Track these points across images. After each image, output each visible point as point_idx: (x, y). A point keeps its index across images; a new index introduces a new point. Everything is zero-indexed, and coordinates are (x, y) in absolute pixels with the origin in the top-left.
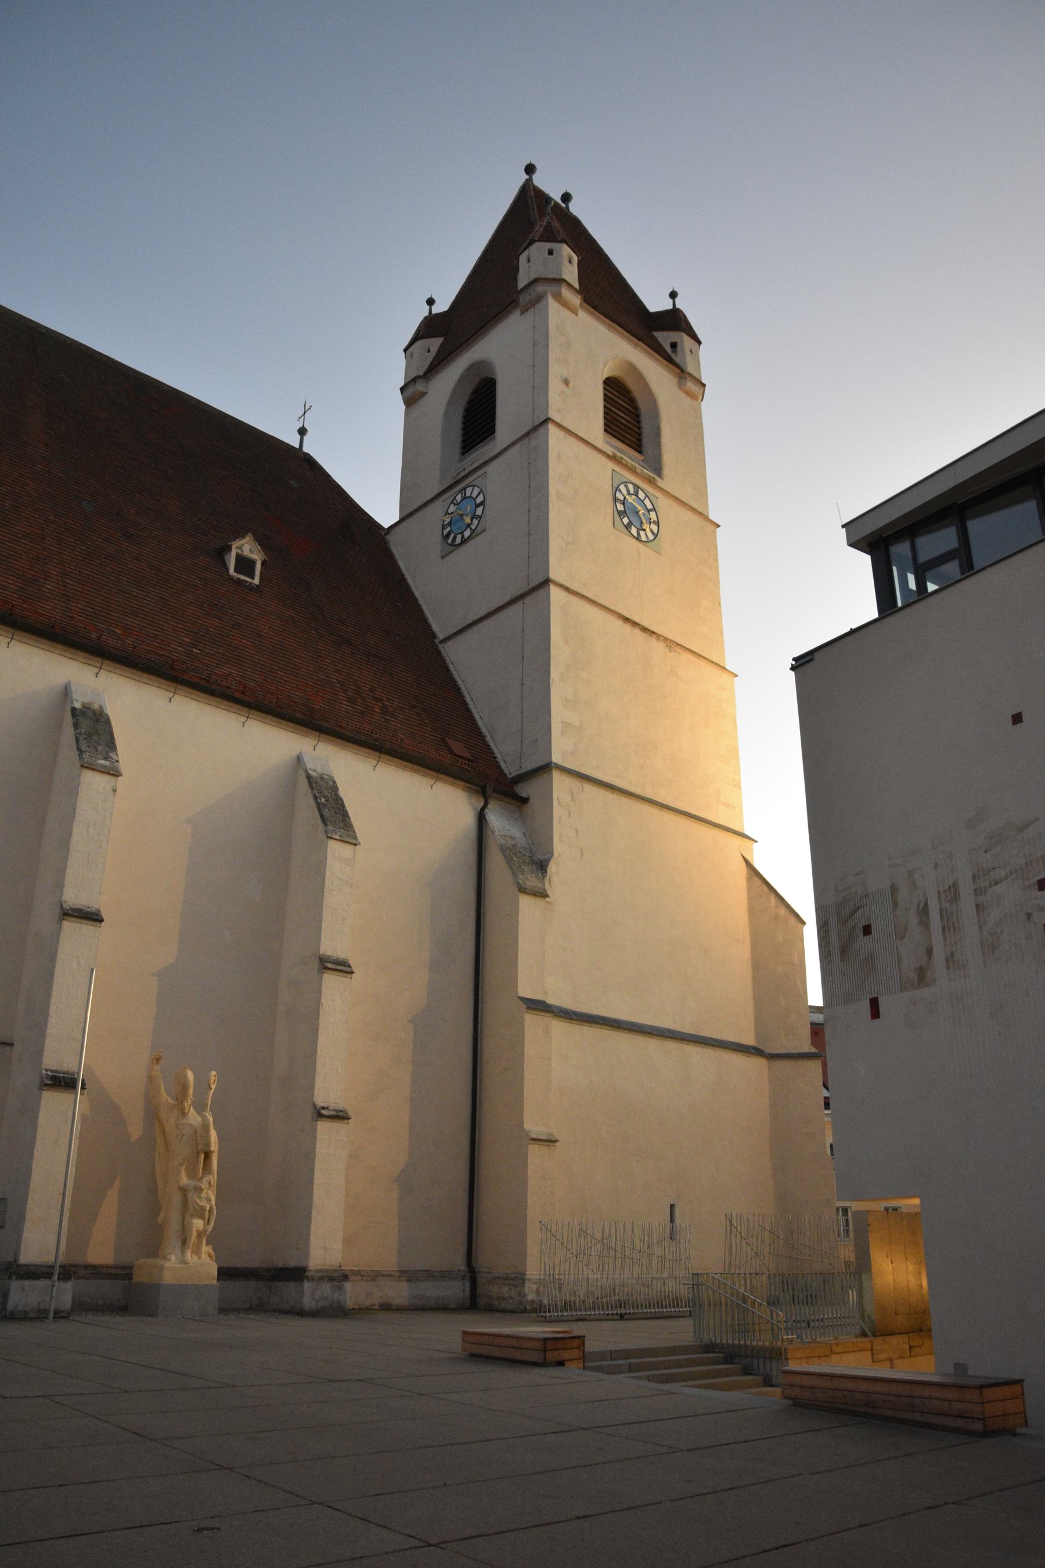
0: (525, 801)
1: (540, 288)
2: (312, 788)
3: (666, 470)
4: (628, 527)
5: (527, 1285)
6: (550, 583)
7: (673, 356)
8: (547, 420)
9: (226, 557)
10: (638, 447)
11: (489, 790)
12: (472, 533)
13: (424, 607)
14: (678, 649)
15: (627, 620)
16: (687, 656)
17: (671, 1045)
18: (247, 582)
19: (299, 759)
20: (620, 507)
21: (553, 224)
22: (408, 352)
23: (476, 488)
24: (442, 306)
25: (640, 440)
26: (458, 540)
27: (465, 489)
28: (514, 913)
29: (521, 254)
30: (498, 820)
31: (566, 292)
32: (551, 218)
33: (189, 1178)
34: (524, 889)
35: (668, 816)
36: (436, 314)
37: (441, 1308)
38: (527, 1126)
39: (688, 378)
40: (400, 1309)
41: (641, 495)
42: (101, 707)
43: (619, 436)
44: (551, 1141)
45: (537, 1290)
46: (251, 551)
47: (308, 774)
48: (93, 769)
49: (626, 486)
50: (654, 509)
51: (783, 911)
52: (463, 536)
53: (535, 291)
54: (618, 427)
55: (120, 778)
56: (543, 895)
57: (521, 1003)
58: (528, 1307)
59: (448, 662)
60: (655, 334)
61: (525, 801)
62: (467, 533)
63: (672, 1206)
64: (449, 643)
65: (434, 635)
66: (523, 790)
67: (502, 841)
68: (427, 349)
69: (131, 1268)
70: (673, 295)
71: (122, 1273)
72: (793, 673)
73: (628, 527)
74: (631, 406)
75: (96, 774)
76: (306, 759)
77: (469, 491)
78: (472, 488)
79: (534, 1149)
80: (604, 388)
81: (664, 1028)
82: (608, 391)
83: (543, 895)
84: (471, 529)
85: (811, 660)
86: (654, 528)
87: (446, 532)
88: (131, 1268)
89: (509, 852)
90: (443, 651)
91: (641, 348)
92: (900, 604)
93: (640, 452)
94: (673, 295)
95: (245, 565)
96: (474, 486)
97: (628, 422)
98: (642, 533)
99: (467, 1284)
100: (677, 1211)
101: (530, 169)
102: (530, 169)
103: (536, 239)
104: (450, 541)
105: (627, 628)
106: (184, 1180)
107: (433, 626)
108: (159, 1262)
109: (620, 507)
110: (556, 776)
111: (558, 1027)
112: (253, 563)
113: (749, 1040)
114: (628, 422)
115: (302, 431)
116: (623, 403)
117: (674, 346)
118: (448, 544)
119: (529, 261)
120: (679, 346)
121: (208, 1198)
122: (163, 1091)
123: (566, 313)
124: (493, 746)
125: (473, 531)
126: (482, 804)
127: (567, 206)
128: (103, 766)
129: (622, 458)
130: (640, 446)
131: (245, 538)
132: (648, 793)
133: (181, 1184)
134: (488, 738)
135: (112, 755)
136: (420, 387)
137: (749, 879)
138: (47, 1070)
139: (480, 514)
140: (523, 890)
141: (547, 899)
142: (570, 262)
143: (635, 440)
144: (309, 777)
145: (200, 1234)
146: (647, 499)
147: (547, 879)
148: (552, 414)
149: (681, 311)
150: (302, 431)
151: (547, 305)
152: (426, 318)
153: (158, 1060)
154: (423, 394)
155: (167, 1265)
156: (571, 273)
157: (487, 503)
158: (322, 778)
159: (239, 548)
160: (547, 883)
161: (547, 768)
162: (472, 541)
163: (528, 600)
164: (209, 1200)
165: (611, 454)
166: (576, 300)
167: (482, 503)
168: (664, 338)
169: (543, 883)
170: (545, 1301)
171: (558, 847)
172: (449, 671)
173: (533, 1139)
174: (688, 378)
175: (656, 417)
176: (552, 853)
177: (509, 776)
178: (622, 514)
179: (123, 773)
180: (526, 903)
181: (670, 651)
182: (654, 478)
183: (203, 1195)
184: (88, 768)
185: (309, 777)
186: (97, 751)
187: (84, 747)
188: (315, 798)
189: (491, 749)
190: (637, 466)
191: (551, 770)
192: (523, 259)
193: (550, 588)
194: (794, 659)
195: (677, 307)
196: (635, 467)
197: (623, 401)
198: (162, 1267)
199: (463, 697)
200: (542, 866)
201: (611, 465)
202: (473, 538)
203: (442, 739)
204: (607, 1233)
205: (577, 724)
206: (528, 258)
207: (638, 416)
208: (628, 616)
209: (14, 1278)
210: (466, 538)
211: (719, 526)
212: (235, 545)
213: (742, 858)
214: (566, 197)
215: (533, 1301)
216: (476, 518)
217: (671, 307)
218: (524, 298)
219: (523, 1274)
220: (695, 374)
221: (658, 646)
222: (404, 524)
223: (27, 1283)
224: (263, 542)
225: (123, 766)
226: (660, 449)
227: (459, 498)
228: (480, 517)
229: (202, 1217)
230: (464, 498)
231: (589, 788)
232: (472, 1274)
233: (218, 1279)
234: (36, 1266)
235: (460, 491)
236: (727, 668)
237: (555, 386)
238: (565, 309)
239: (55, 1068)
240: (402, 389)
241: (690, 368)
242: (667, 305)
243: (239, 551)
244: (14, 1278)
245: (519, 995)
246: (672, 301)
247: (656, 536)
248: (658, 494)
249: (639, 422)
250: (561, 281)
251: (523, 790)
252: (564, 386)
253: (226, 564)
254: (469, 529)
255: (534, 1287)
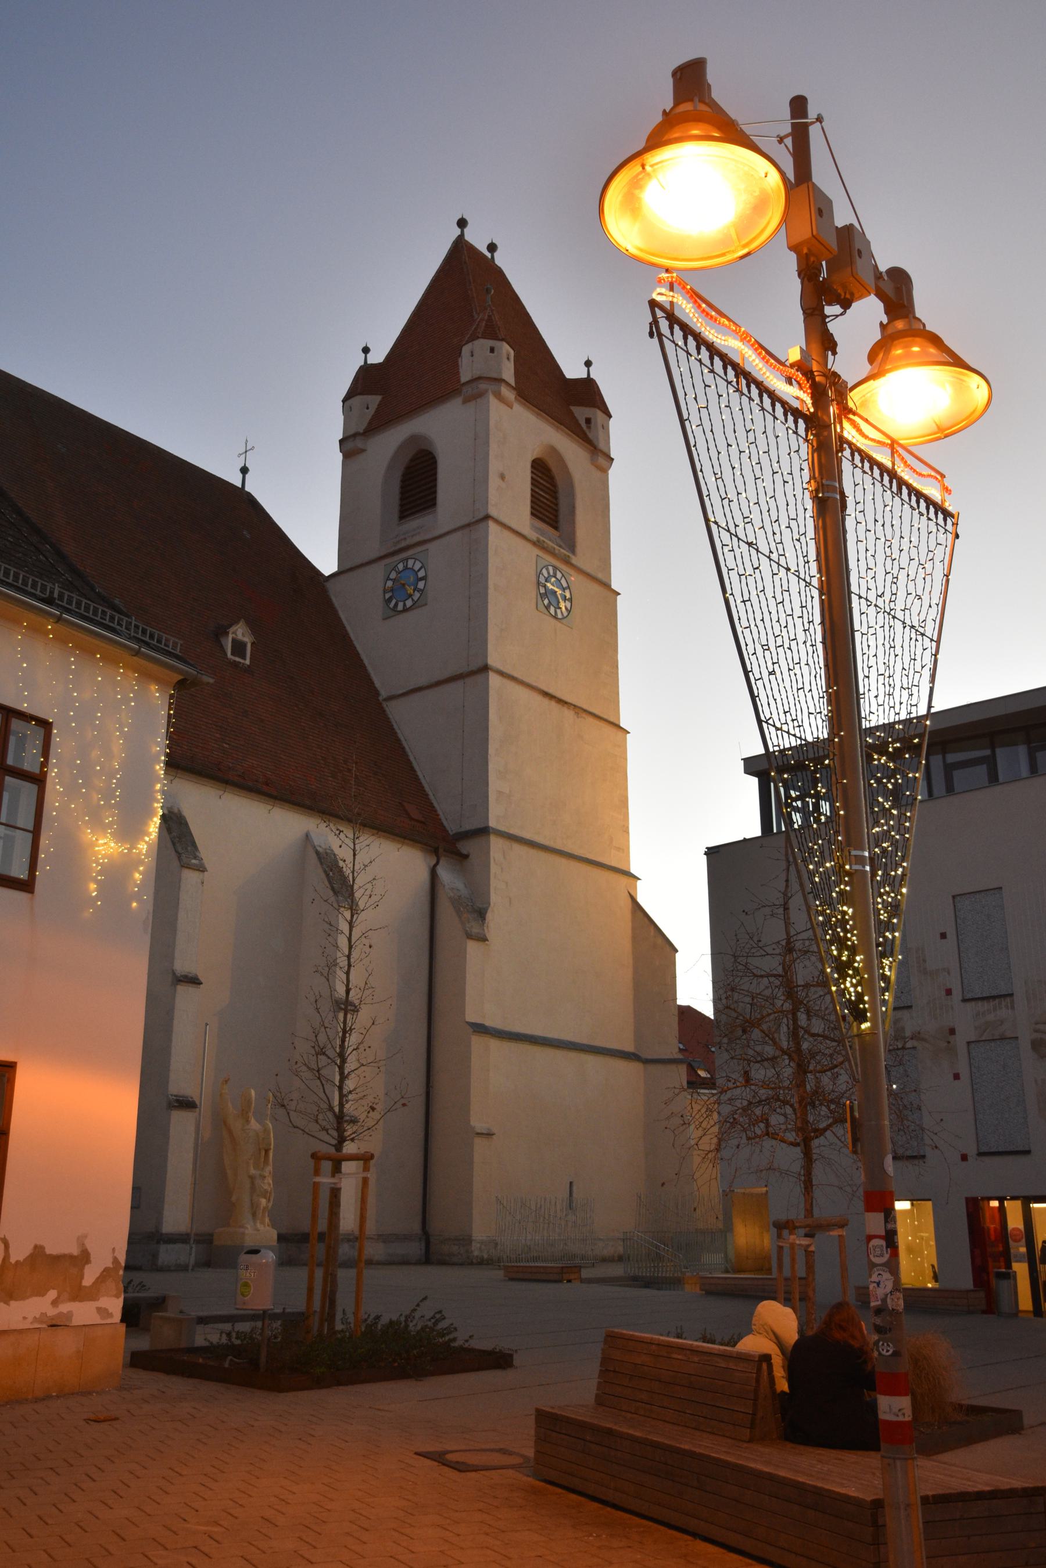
0: (466, 857)
1: (483, 386)
2: (321, 864)
3: (579, 548)
4: (547, 608)
5: (474, 1244)
6: (490, 672)
7: (588, 433)
8: (487, 517)
9: (223, 640)
10: (554, 524)
11: (441, 851)
12: (414, 604)
13: (366, 662)
14: (584, 715)
15: (546, 694)
16: (590, 720)
17: (572, 1055)
18: (240, 663)
19: (307, 836)
20: (542, 590)
21: (493, 318)
22: (348, 403)
23: (417, 562)
24: (377, 357)
25: (556, 516)
26: (400, 607)
27: (407, 559)
28: (462, 955)
29: (464, 345)
30: (445, 874)
31: (505, 391)
32: (492, 311)
33: (254, 1169)
34: (471, 935)
35: (574, 865)
36: (372, 364)
37: (405, 1262)
38: (472, 1123)
39: (599, 454)
40: (379, 1263)
41: (559, 575)
42: (179, 811)
43: (541, 516)
44: (489, 1135)
45: (480, 1248)
46: (243, 635)
47: (317, 850)
48: (190, 868)
49: (547, 570)
50: (568, 587)
51: (660, 941)
52: (405, 605)
53: (478, 388)
54: (540, 506)
55: (206, 873)
56: (483, 939)
57: (468, 1027)
58: (474, 1261)
59: (392, 720)
60: (572, 408)
61: (466, 857)
62: (409, 603)
63: (571, 1183)
64: (393, 703)
65: (377, 693)
66: (464, 847)
67: (452, 894)
68: (366, 406)
69: (212, 1235)
70: (588, 364)
71: (206, 1240)
72: (705, 856)
73: (547, 608)
74: (551, 485)
75: (191, 871)
76: (313, 835)
77: (410, 563)
78: (413, 560)
79: (478, 1141)
80: (532, 472)
81: (567, 1041)
82: (535, 474)
83: (483, 939)
84: (413, 600)
85: (718, 852)
86: (568, 604)
87: (387, 596)
88: (212, 1235)
89: (457, 902)
90: (387, 709)
91: (563, 430)
92: (775, 831)
93: (556, 528)
94: (588, 364)
95: (239, 648)
96: (416, 559)
97: (547, 499)
98: (558, 611)
99: (423, 1244)
100: (575, 1188)
101: (462, 223)
102: (462, 223)
103: (480, 336)
104: (392, 605)
105: (546, 702)
106: (253, 1171)
107: (375, 682)
108: (242, 1230)
109: (542, 590)
110: (493, 839)
111: (494, 1043)
112: (243, 645)
113: (629, 1047)
114: (547, 499)
115: (244, 470)
116: (544, 483)
117: (588, 421)
118: (390, 608)
119: (472, 356)
120: (593, 421)
121: (268, 1184)
122: (230, 1105)
123: (503, 407)
124: (436, 805)
125: (415, 603)
126: (434, 862)
127: (493, 257)
128: (195, 865)
129: (544, 542)
130: (557, 522)
131: (238, 624)
132: (559, 846)
133: (251, 1174)
134: (431, 797)
135: (197, 854)
136: (359, 443)
137: (633, 913)
138: (172, 1095)
139: (422, 588)
140: (470, 936)
141: (487, 942)
142: (508, 359)
143: (551, 516)
144: (317, 853)
145: (264, 1208)
146: (563, 579)
147: (485, 925)
148: (493, 511)
149: (595, 381)
150: (244, 470)
151: (488, 402)
152: (361, 367)
153: (226, 1081)
154: (363, 451)
155: (247, 1232)
156: (508, 373)
157: (429, 578)
158: (326, 853)
159: (234, 633)
160: (485, 928)
161: (484, 831)
162: (414, 611)
163: (469, 681)
164: (269, 1185)
165: (535, 539)
166: (509, 394)
167: (424, 578)
168: (581, 413)
169: (483, 930)
170: (486, 1256)
171: (493, 898)
172: (394, 729)
173: (478, 1134)
174: (599, 454)
175: (572, 495)
176: (490, 904)
177: (451, 834)
178: (543, 596)
179: (208, 869)
180: (472, 946)
181: (578, 717)
182: (569, 556)
183: (266, 1181)
184: (187, 867)
185: (317, 853)
186: (187, 851)
187: (180, 850)
188: (325, 872)
189: (434, 807)
190: (555, 546)
191: (489, 835)
192: (466, 350)
193: (488, 675)
194: (707, 848)
195: (592, 376)
196: (554, 549)
197: (544, 480)
198: (243, 1234)
199: (408, 756)
200: (481, 914)
201: (536, 551)
202: (413, 609)
203: (400, 803)
204: (539, 1206)
205: (508, 792)
206: (472, 352)
207: (556, 492)
208: (546, 689)
209: (162, 1242)
210: (408, 607)
211: (619, 594)
212: (231, 630)
213: (630, 900)
214: (492, 247)
215: (477, 1256)
216: (418, 591)
217: (585, 376)
218: (468, 391)
219: (470, 1236)
220: (605, 449)
221: (568, 714)
222: (342, 577)
223: (170, 1246)
224: (254, 627)
225: (206, 862)
226: (574, 527)
227: (401, 567)
228: (422, 590)
229: (265, 1198)
230: (406, 568)
231: (517, 847)
232: (426, 1235)
233: (278, 1243)
234: (172, 1234)
235: (402, 561)
236: (621, 725)
237: (494, 482)
238: (502, 404)
239: (175, 1094)
240: (341, 441)
241: (601, 445)
242: (579, 373)
243: (234, 635)
244: (162, 1242)
245: (467, 1020)
246: (586, 369)
247: (570, 611)
248: (572, 572)
249: (556, 498)
250: (502, 381)
251: (464, 847)
252: (501, 481)
253: (223, 648)
254: (410, 599)
255: (478, 1245)
